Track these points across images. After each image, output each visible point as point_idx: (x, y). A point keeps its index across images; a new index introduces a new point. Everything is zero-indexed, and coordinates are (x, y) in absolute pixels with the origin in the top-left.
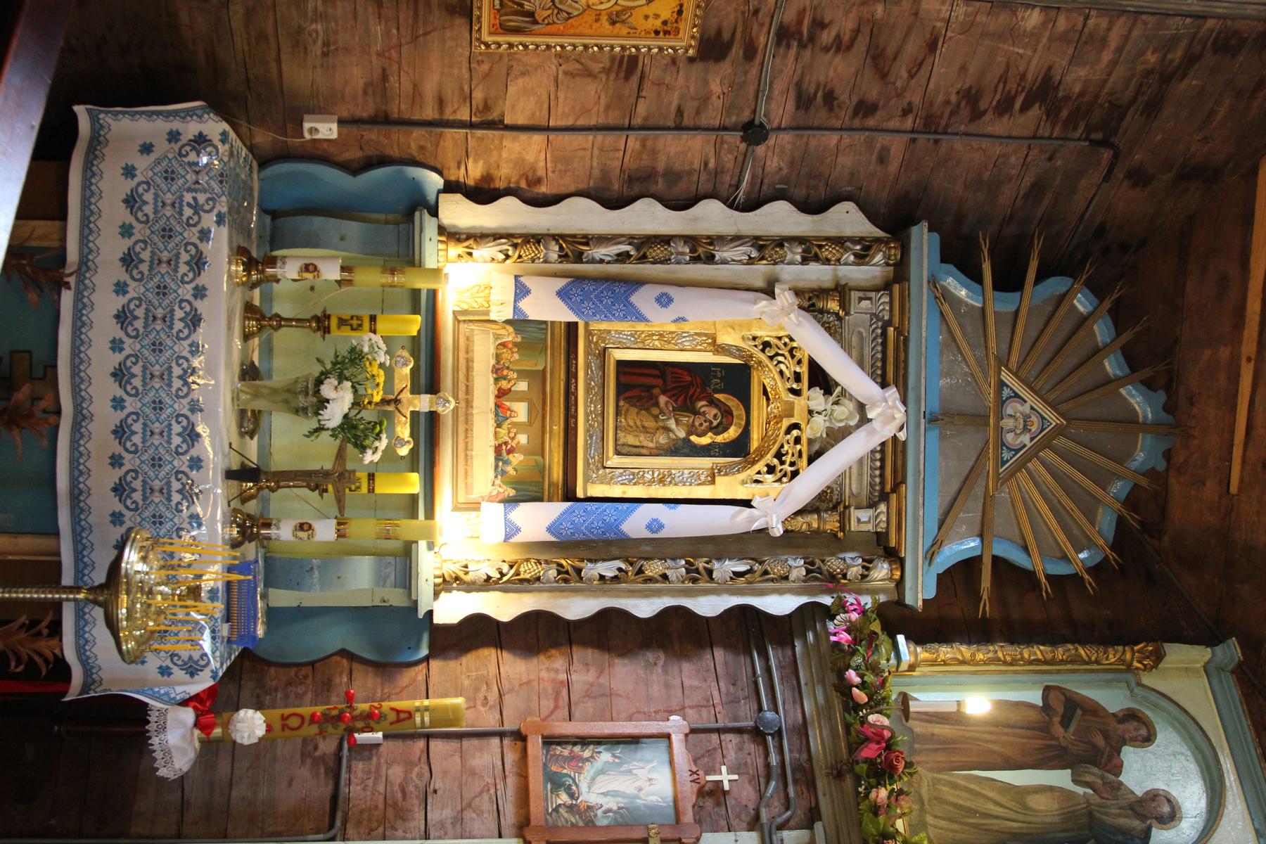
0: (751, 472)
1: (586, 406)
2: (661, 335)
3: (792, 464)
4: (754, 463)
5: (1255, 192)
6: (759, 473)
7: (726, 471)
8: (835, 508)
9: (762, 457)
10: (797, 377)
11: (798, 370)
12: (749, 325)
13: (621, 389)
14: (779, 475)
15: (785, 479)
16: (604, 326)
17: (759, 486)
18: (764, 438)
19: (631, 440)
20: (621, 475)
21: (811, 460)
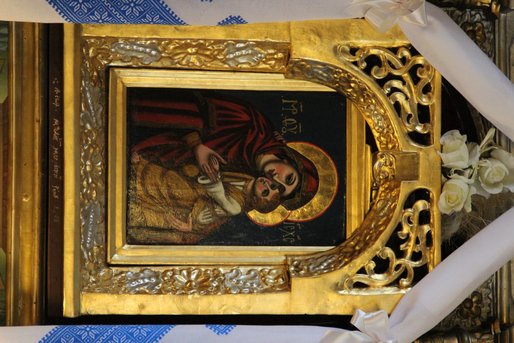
0: (349, 270)
1: (78, 165)
2: (201, 47)
3: (416, 256)
4: (353, 254)
5: (249, 245)
6: (362, 271)
7: (308, 268)
8: (485, 327)
9: (367, 245)
10: (424, 114)
11: (425, 101)
12: (344, 30)
13: (135, 136)
14: (395, 274)
15: (405, 282)
16: (106, 31)
17: (363, 293)
18: (367, 215)
19: (153, 219)
20: (136, 277)
21: (446, 251)
